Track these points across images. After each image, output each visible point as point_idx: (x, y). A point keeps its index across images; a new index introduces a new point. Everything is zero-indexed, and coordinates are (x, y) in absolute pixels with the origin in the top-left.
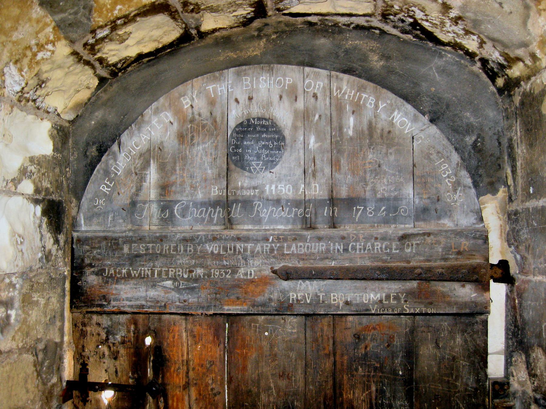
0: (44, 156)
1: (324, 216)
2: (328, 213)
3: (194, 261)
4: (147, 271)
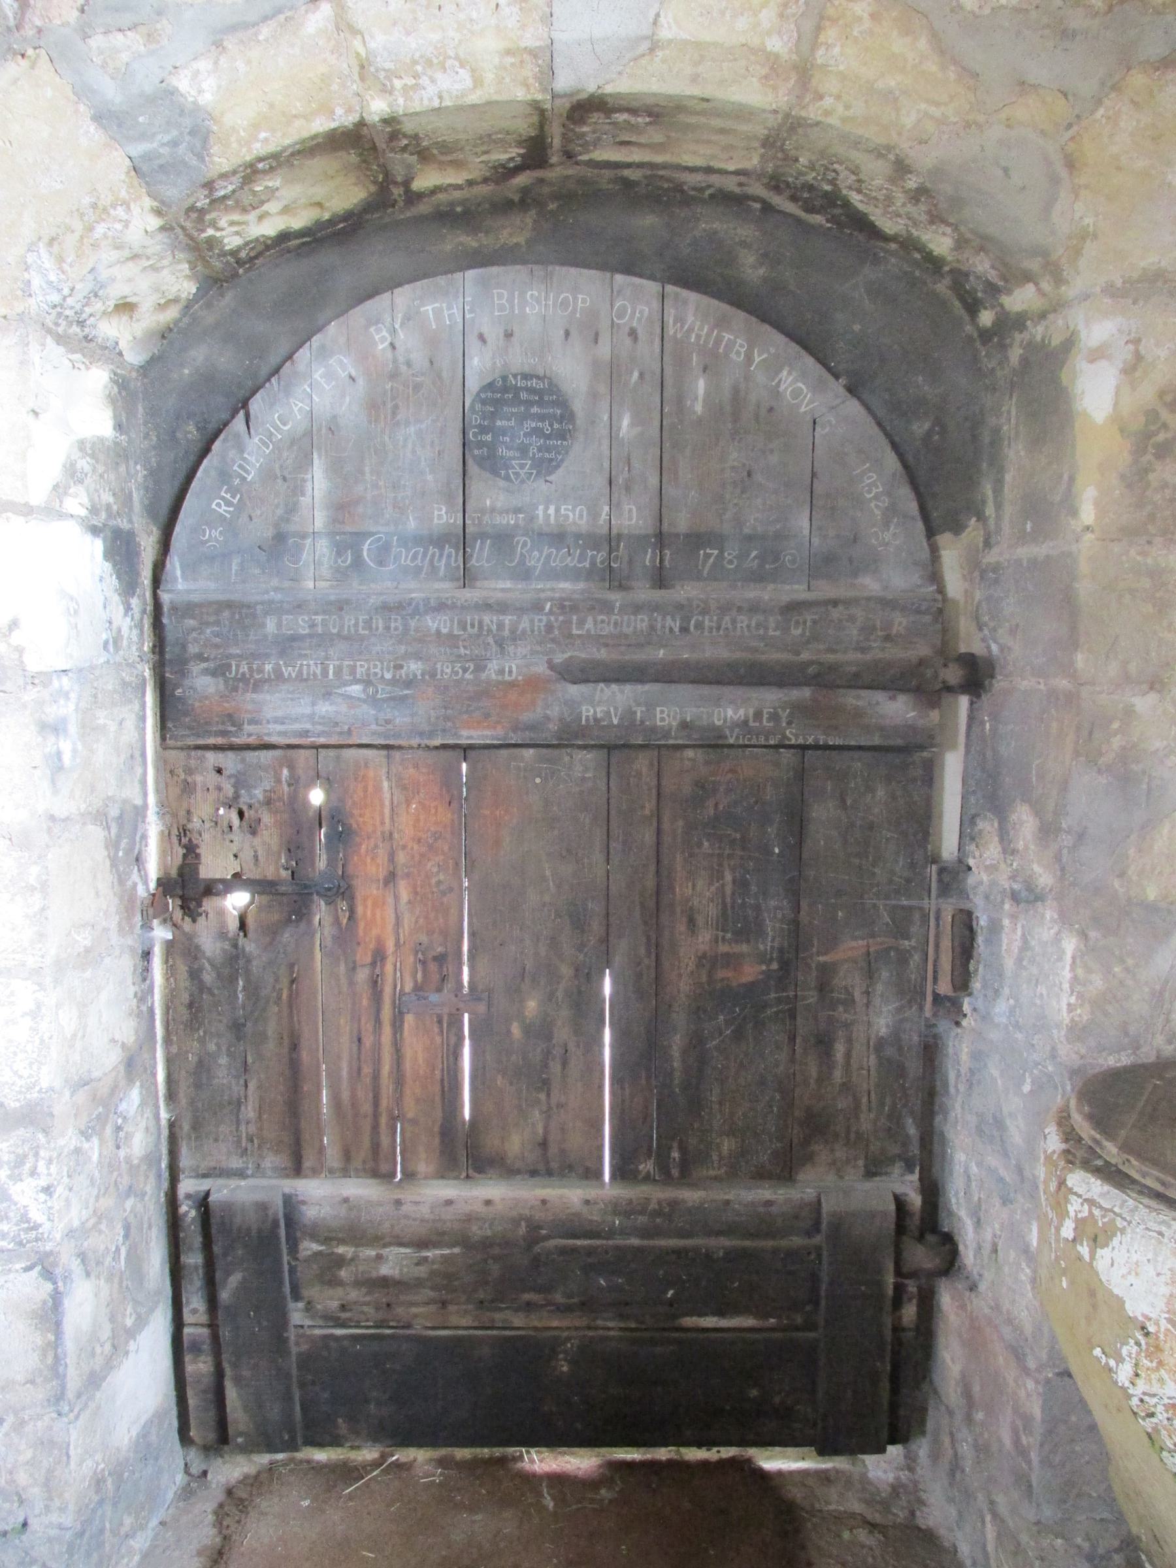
0: (102, 440)
1: (645, 566)
2: (653, 560)
3: (403, 647)
4: (313, 668)
